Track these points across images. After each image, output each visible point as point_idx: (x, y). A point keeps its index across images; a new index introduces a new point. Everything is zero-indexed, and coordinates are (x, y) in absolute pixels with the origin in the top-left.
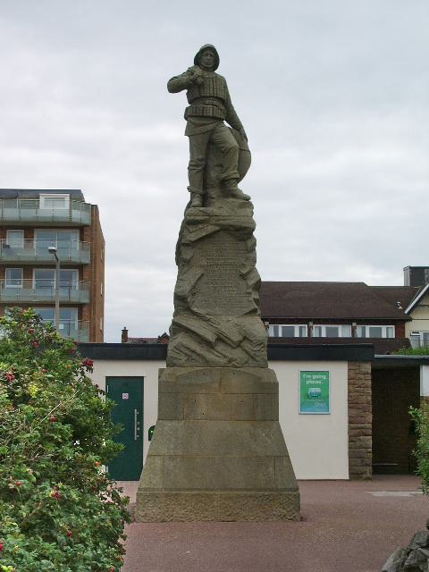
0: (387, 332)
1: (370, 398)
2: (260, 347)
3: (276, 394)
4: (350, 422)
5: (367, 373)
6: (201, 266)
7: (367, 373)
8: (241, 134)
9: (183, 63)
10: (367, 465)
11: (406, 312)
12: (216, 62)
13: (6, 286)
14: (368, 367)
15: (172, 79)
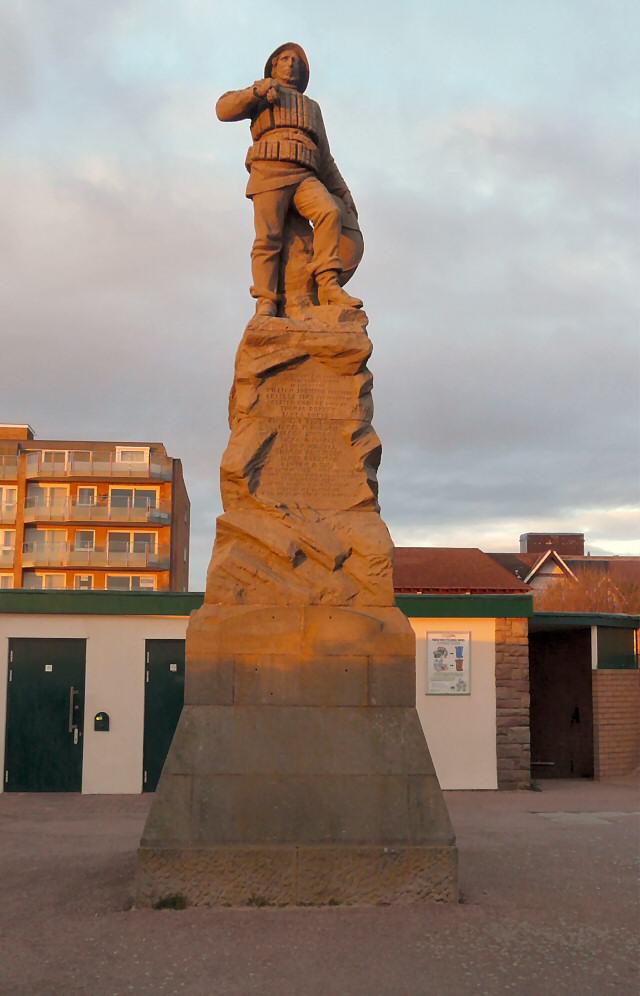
4: (498, 707)
8: (346, 203)
9: (248, 75)
10: (522, 768)
11: (526, 581)
12: (300, 75)
13: (76, 549)
14: (520, 628)
15: (222, 97)
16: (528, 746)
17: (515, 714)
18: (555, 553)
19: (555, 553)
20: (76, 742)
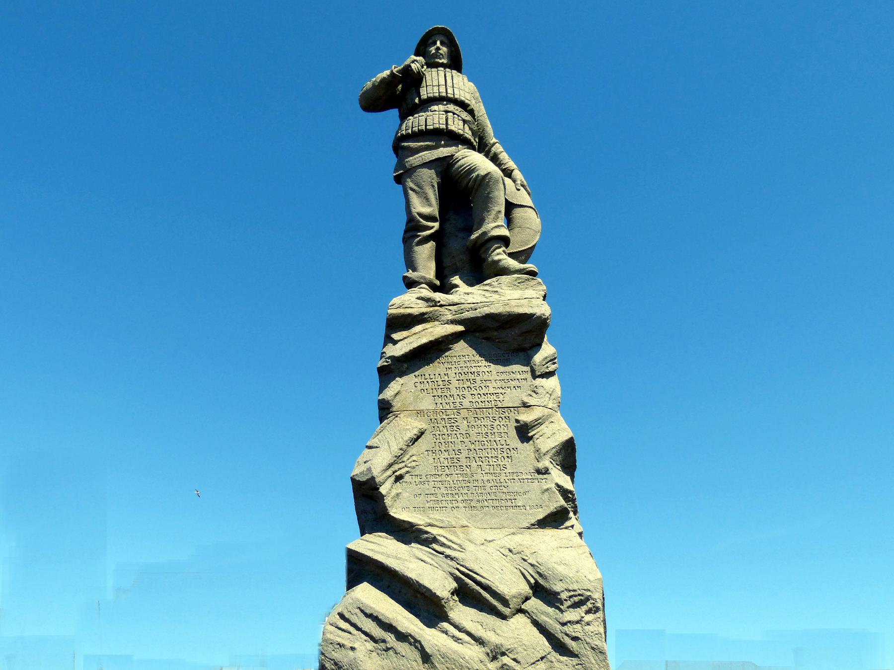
6: (419, 413)
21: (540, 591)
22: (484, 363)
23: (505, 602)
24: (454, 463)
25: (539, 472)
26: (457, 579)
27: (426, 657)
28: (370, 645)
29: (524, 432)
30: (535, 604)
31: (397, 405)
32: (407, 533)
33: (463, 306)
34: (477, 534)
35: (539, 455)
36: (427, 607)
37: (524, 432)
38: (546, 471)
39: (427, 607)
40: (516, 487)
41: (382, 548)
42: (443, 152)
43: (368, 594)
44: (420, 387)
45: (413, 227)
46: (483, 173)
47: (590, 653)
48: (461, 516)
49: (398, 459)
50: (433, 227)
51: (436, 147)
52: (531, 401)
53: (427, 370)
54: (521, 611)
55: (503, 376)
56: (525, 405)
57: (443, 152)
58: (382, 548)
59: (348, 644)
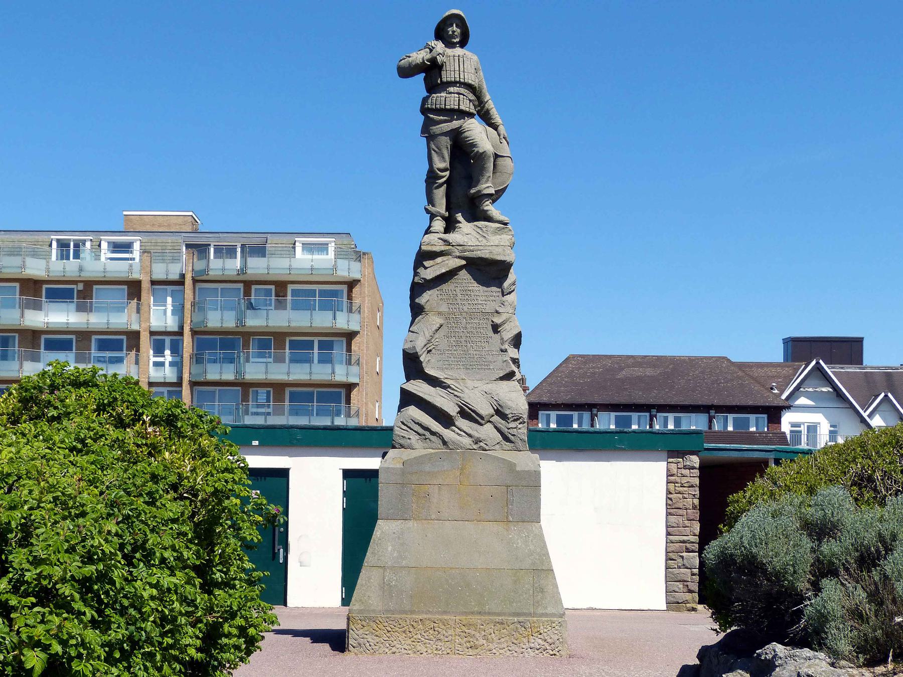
0: (755, 424)
1: (696, 502)
2: (517, 423)
3: (537, 486)
5: (693, 468)
6: (440, 313)
7: (693, 468)
10: (690, 591)
11: (784, 397)
16: (696, 571)
17: (684, 542)
18: (821, 362)
19: (821, 362)
20: (281, 561)
21: (499, 413)
22: (476, 285)
23: (482, 418)
24: (458, 344)
25: (502, 351)
26: (459, 406)
27: (445, 443)
28: (418, 437)
29: (496, 328)
30: (496, 419)
31: (427, 308)
32: (434, 382)
33: (466, 248)
34: (470, 383)
35: (503, 342)
36: (445, 419)
37: (496, 328)
38: (506, 351)
39: (445, 419)
40: (490, 358)
41: (419, 388)
42: (455, 124)
43: (413, 412)
44: (440, 297)
45: (432, 177)
46: (481, 151)
47: (520, 442)
48: (462, 374)
49: (429, 341)
50: (443, 177)
51: (451, 121)
52: (500, 310)
53: (444, 287)
54: (490, 421)
55: (486, 294)
56: (497, 312)
57: (455, 124)
58: (419, 388)
59: (407, 437)
